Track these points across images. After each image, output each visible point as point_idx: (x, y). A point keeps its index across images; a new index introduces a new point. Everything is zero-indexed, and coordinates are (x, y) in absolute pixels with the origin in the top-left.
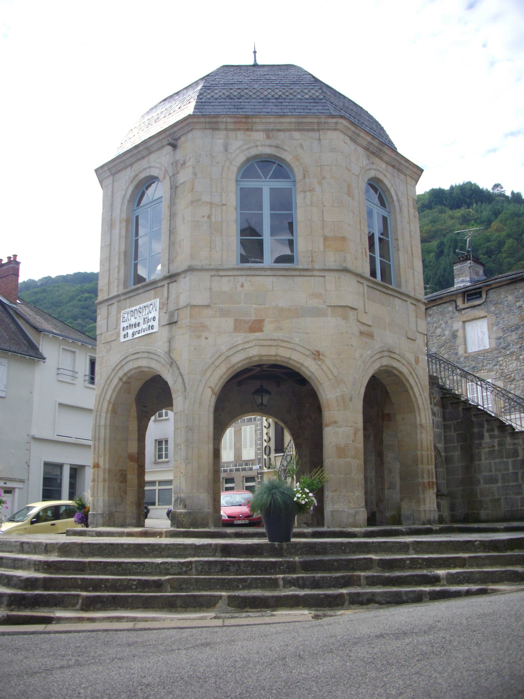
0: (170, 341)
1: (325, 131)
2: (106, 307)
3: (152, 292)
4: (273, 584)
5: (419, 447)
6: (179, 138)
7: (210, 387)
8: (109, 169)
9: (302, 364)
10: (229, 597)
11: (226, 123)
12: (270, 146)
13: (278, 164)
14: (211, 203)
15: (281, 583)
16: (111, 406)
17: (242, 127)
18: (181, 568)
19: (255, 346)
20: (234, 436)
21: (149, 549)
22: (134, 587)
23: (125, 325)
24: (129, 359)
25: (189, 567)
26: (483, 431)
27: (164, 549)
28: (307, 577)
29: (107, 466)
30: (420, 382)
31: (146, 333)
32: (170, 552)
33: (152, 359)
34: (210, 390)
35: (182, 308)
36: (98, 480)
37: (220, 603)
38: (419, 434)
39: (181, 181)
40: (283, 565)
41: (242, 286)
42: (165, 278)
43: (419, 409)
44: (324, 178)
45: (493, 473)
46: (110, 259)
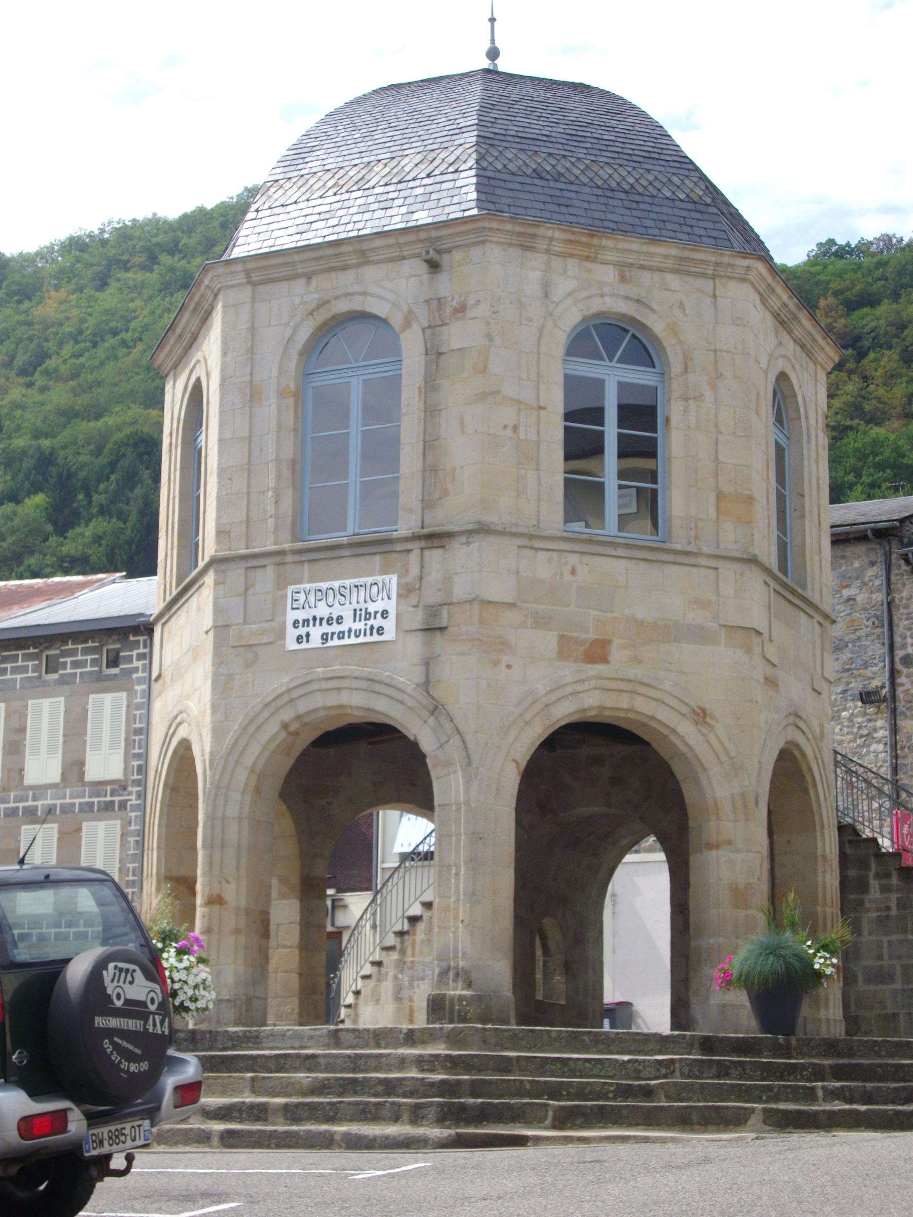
0: (428, 663)
1: (724, 280)
2: (243, 571)
3: (377, 558)
4: (810, 1095)
5: (820, 900)
6: (449, 251)
7: (515, 761)
8: (248, 273)
9: (673, 731)
10: (765, 1110)
11: (551, 239)
12: (627, 298)
13: (634, 336)
14: (520, 402)
15: (820, 1093)
16: (254, 779)
17: (577, 252)
18: (659, 1070)
19: (595, 688)
20: (59, 847)
21: (590, 1040)
22: (611, 1095)
23: (301, 615)
24: (315, 686)
25: (669, 1068)
26: (867, 876)
27: (613, 1041)
28: (856, 1087)
29: (243, 903)
30: (826, 775)
31: (361, 639)
32: (623, 1045)
33: (379, 693)
34: (513, 765)
35: (459, 603)
36: (220, 931)
37: (753, 1120)
38: (820, 874)
39: (455, 345)
40: (806, 1070)
41: (573, 572)
42: (415, 538)
43: (823, 827)
44: (719, 376)
45: (886, 962)
46: (249, 470)
